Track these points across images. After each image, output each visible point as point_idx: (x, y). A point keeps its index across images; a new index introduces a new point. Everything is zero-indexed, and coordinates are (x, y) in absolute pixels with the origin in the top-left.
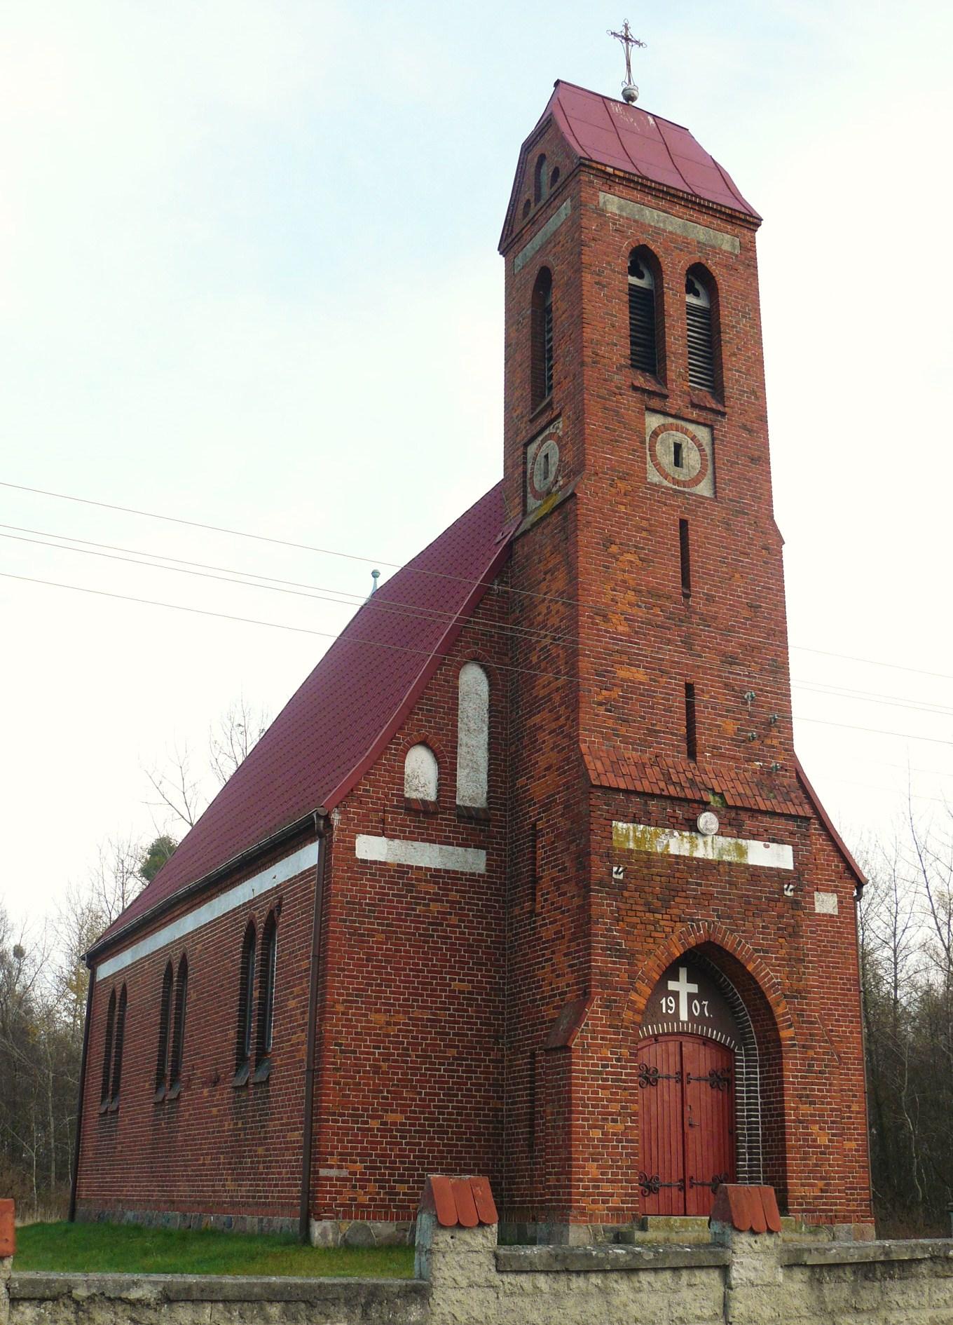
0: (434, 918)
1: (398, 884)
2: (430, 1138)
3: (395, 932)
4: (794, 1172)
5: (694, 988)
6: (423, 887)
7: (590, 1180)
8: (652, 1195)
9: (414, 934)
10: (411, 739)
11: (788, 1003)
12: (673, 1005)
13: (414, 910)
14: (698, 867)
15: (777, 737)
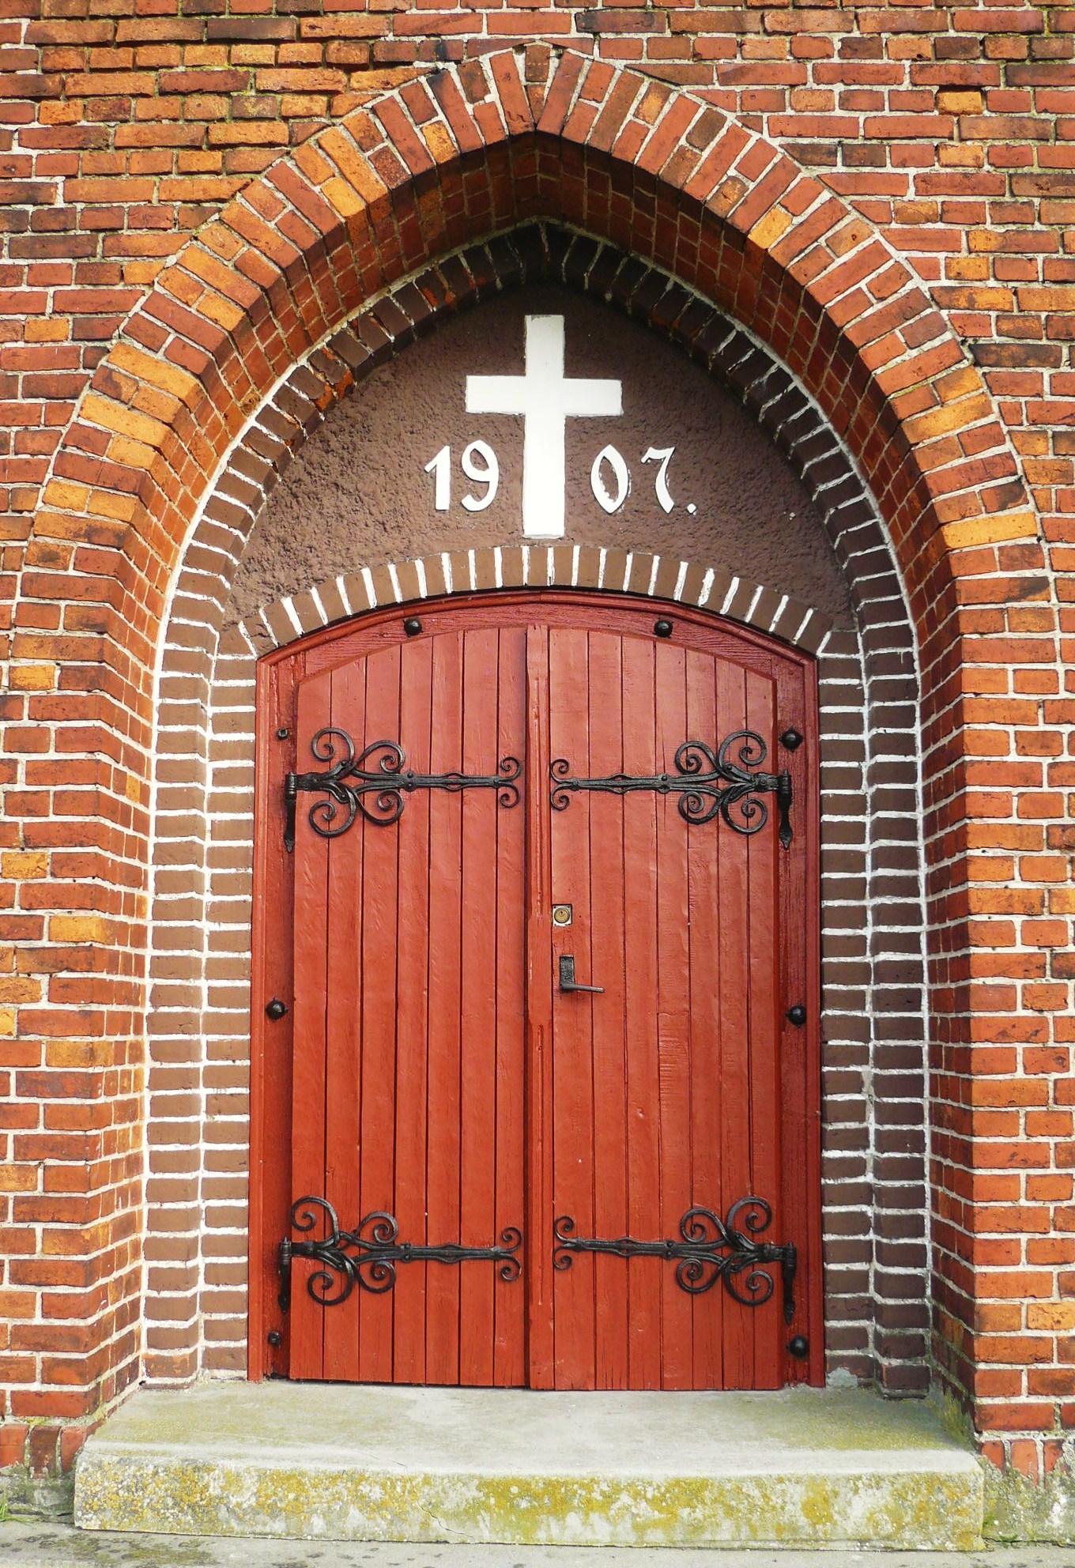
4: (1018, 1220)
8: (367, 1304)
11: (994, 386)
12: (492, 475)
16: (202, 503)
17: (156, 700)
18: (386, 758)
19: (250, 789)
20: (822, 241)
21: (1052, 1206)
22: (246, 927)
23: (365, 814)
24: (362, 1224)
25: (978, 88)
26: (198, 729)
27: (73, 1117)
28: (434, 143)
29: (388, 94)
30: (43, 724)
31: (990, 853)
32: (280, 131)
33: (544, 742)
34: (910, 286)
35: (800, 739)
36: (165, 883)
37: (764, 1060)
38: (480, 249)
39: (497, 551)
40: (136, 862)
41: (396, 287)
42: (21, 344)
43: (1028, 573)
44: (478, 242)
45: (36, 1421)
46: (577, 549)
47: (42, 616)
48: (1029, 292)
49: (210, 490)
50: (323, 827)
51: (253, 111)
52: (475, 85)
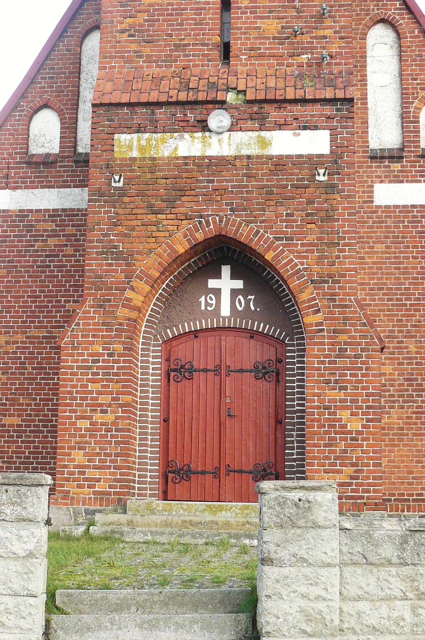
0: (51, 251)
1: (19, 226)
2: (44, 437)
3: (16, 267)
4: (315, 458)
5: (239, 284)
6: (41, 226)
7: (75, 467)
9: (32, 267)
10: (35, 105)
11: (315, 288)
12: (214, 302)
13: (33, 246)
14: (210, 164)
15: (331, 27)
16: (150, 309)
17: (140, 352)
18: (190, 365)
19: (160, 372)
20: (280, 258)
21: (322, 455)
22: (159, 402)
23: (185, 377)
24: (184, 466)
25: (314, 223)
26: (149, 358)
27: (126, 437)
28: (199, 237)
29: (190, 226)
30: (120, 358)
31: (311, 385)
32: (167, 234)
33: (225, 361)
34: (298, 267)
35: (282, 361)
36: (142, 392)
37: (272, 430)
38: (211, 252)
39: (215, 319)
40: (136, 387)
41: (192, 260)
42: (114, 279)
43: (320, 328)
44: (210, 250)
45: (118, 497)
46: (232, 319)
47: (120, 336)
48: (323, 268)
49: (151, 306)
50: (176, 380)
51: (161, 230)
52: (208, 224)
